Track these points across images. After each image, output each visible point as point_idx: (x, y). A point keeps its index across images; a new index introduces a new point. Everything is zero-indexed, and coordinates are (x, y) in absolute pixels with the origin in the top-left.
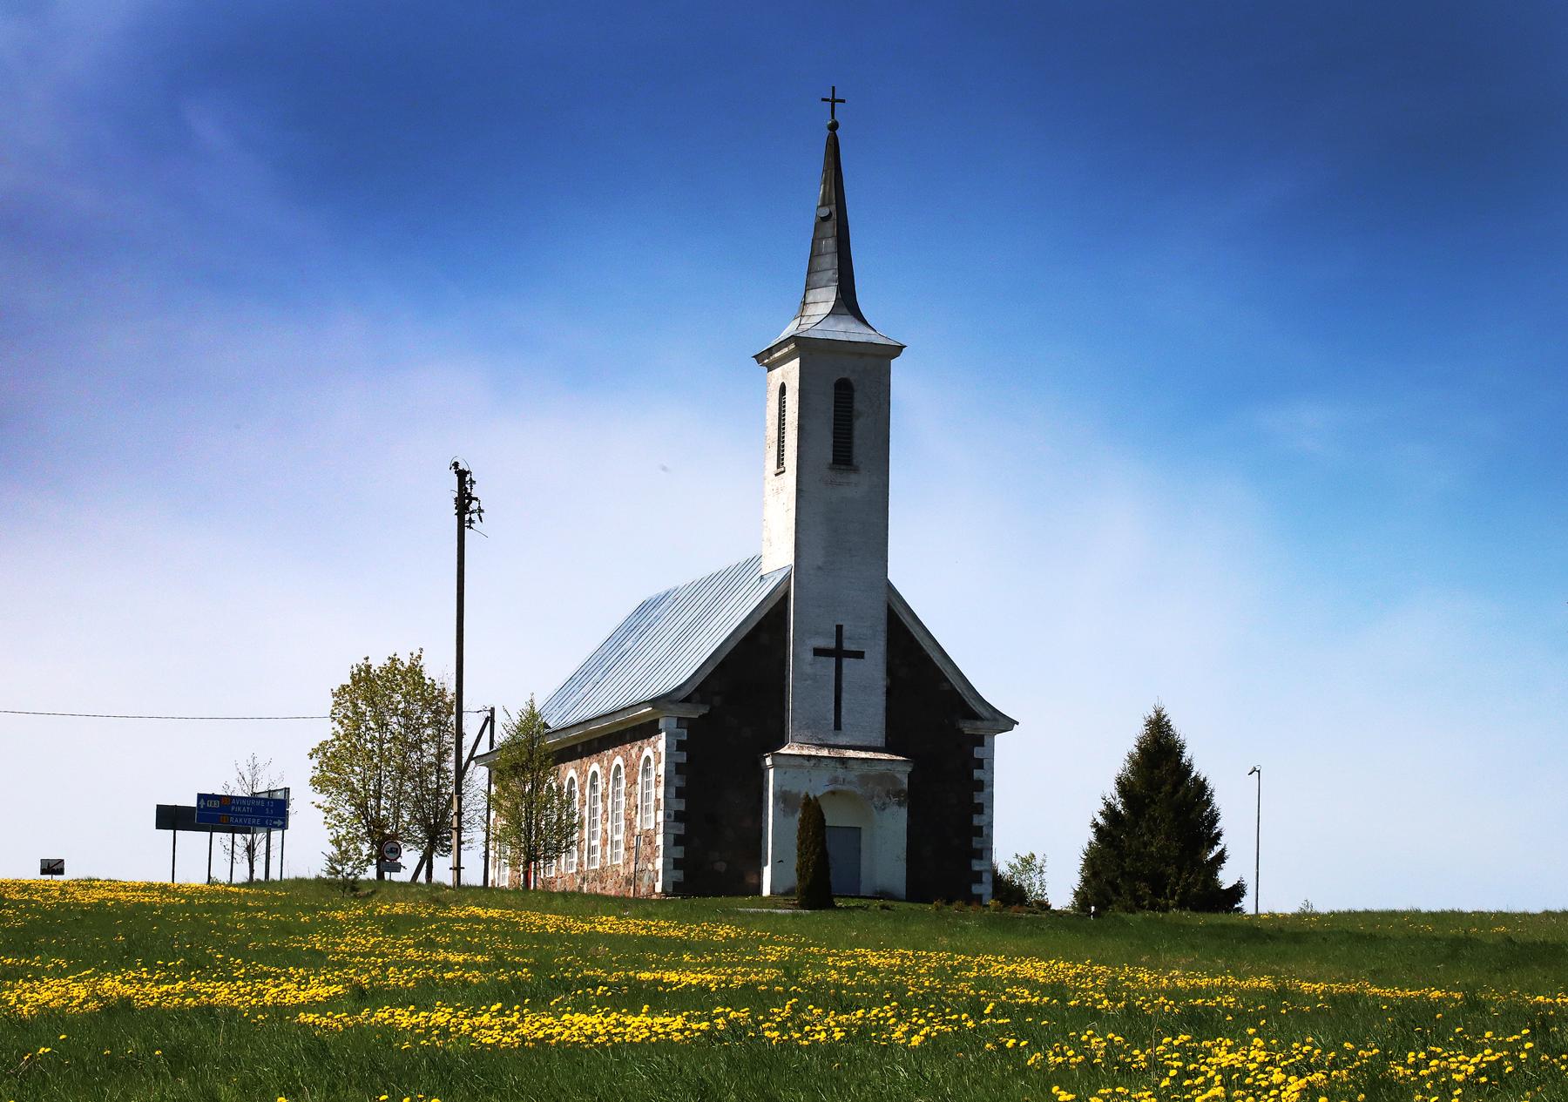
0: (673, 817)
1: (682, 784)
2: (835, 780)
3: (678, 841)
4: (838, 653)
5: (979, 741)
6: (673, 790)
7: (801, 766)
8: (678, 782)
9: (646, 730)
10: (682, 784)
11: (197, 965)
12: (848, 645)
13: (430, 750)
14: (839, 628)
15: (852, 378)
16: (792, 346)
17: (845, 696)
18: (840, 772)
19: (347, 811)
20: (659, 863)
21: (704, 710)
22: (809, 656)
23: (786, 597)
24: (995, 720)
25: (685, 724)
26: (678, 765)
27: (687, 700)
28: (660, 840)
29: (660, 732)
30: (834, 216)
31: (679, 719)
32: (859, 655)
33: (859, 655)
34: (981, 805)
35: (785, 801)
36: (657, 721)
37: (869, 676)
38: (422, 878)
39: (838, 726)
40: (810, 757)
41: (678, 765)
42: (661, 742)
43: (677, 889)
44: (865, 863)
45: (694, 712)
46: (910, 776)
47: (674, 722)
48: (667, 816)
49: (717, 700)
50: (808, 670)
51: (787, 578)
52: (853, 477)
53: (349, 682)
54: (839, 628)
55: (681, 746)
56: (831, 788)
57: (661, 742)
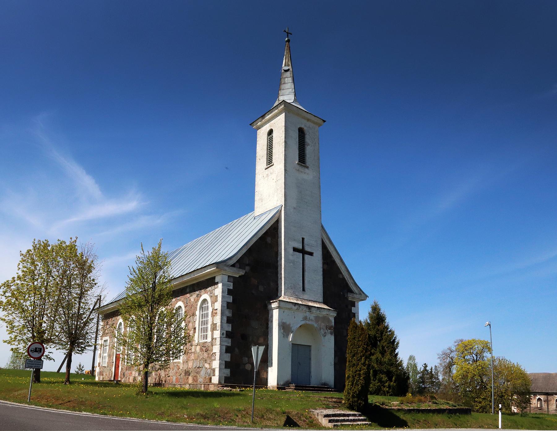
0: (227, 335)
1: (230, 315)
2: (305, 318)
3: (228, 350)
4: (303, 251)
5: (353, 304)
6: (225, 319)
7: (290, 309)
8: (228, 313)
9: (210, 282)
10: (230, 315)
11: (348, 417)
12: (307, 249)
13: (76, 291)
14: (303, 239)
15: (305, 128)
16: (283, 106)
17: (306, 273)
18: (308, 314)
19: (19, 322)
20: (216, 364)
21: (242, 273)
22: (292, 250)
23: (278, 222)
24: (360, 294)
25: (232, 280)
26: (228, 303)
27: (233, 266)
28: (216, 349)
29: (217, 283)
30: (291, 70)
31: (229, 276)
32: (311, 254)
33: (311, 254)
34: (226, 367)
35: (284, 328)
36: (214, 278)
37: (315, 263)
38: (64, 370)
39: (304, 290)
40: (295, 304)
41: (228, 303)
42: (218, 290)
43: (226, 381)
44: (313, 370)
45: (238, 273)
46: (335, 318)
47: (226, 278)
48: (222, 334)
49: (248, 268)
50: (291, 257)
51: (279, 212)
52: (306, 170)
53: (31, 248)
54: (303, 239)
55: (230, 292)
56: (303, 323)
57: (218, 290)
